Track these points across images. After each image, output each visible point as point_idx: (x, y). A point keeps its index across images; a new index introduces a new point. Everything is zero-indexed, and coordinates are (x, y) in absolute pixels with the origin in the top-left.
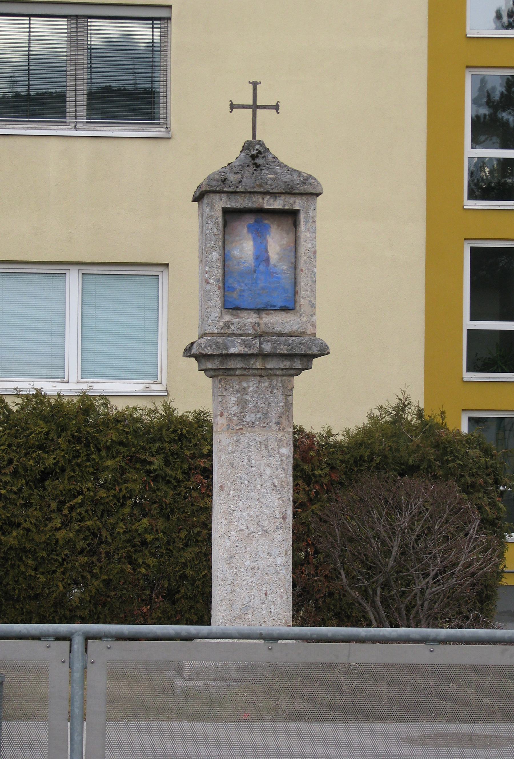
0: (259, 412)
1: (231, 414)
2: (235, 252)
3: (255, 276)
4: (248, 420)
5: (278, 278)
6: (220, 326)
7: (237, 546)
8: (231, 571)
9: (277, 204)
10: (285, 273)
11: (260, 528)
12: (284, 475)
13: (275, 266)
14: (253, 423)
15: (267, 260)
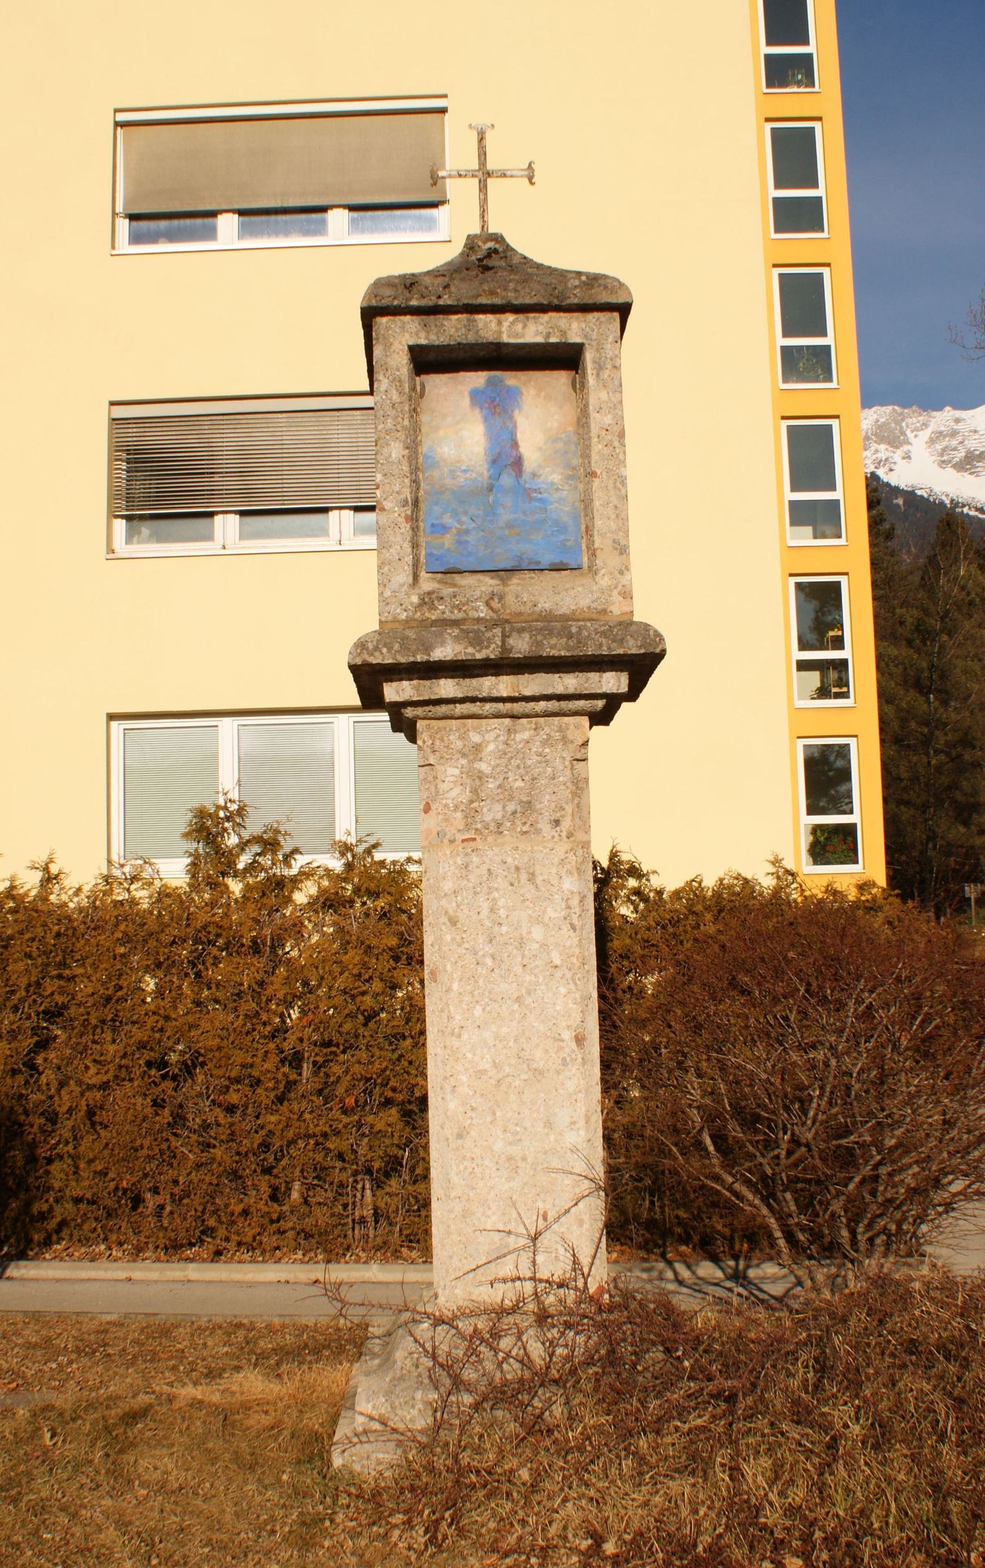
0: (511, 799)
1: (446, 806)
2: (446, 449)
3: (491, 499)
4: (488, 818)
5: (541, 500)
6: (412, 604)
7: (473, 1109)
8: (462, 1167)
9: (531, 331)
10: (557, 489)
11: (525, 1066)
12: (576, 941)
13: (534, 475)
14: (499, 825)
15: (518, 463)
